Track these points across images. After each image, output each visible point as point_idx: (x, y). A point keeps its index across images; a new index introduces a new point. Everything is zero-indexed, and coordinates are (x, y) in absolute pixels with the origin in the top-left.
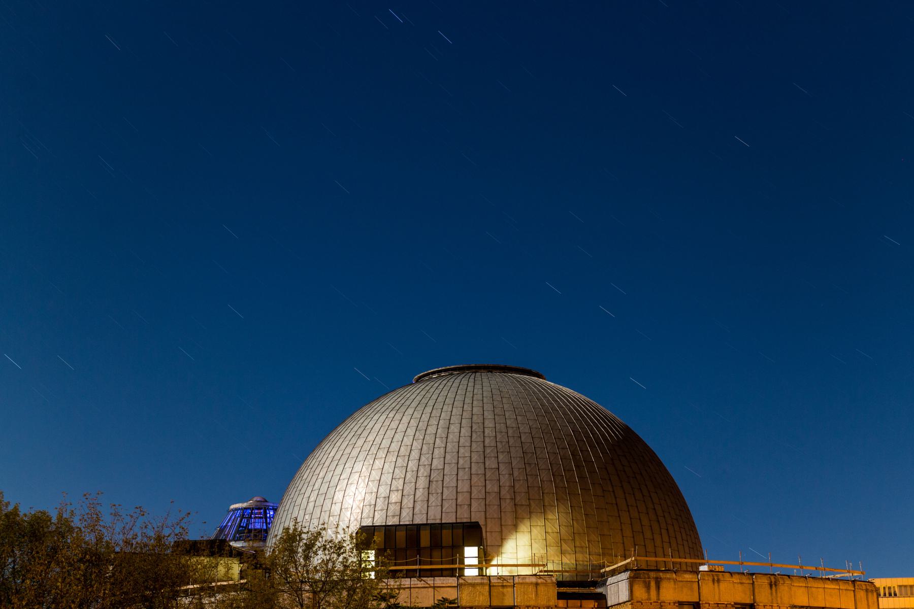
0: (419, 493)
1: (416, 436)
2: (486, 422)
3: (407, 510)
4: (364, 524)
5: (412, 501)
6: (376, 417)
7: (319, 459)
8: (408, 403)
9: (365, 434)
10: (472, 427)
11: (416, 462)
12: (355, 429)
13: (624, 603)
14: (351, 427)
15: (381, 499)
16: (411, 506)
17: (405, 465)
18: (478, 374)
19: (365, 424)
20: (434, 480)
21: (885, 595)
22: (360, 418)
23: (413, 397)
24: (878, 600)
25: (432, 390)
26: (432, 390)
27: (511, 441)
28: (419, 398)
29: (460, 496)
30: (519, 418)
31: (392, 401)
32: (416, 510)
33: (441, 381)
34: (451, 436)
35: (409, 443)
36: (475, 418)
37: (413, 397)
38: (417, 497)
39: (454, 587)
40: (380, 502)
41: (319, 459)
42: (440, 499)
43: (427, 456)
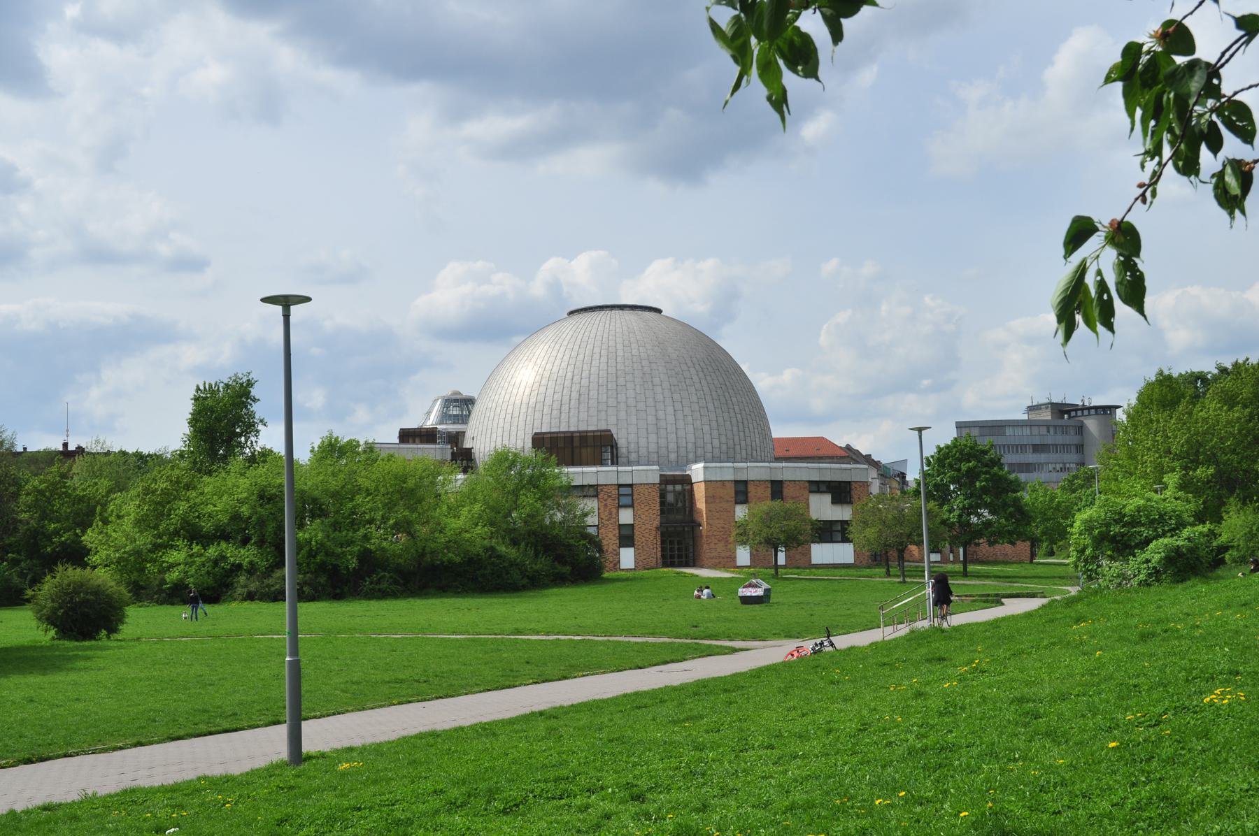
0: (573, 402)
2: (618, 352)
8: (564, 336)
9: (534, 359)
11: (570, 381)
12: (528, 354)
18: (613, 312)
21: (1004, 447)
23: (567, 331)
24: (623, 570)
25: (581, 326)
26: (581, 326)
27: (635, 365)
28: (571, 333)
29: (574, 385)
30: (641, 348)
32: (571, 414)
34: (594, 362)
35: (565, 367)
37: (567, 331)
39: (287, 317)
40: (555, 412)
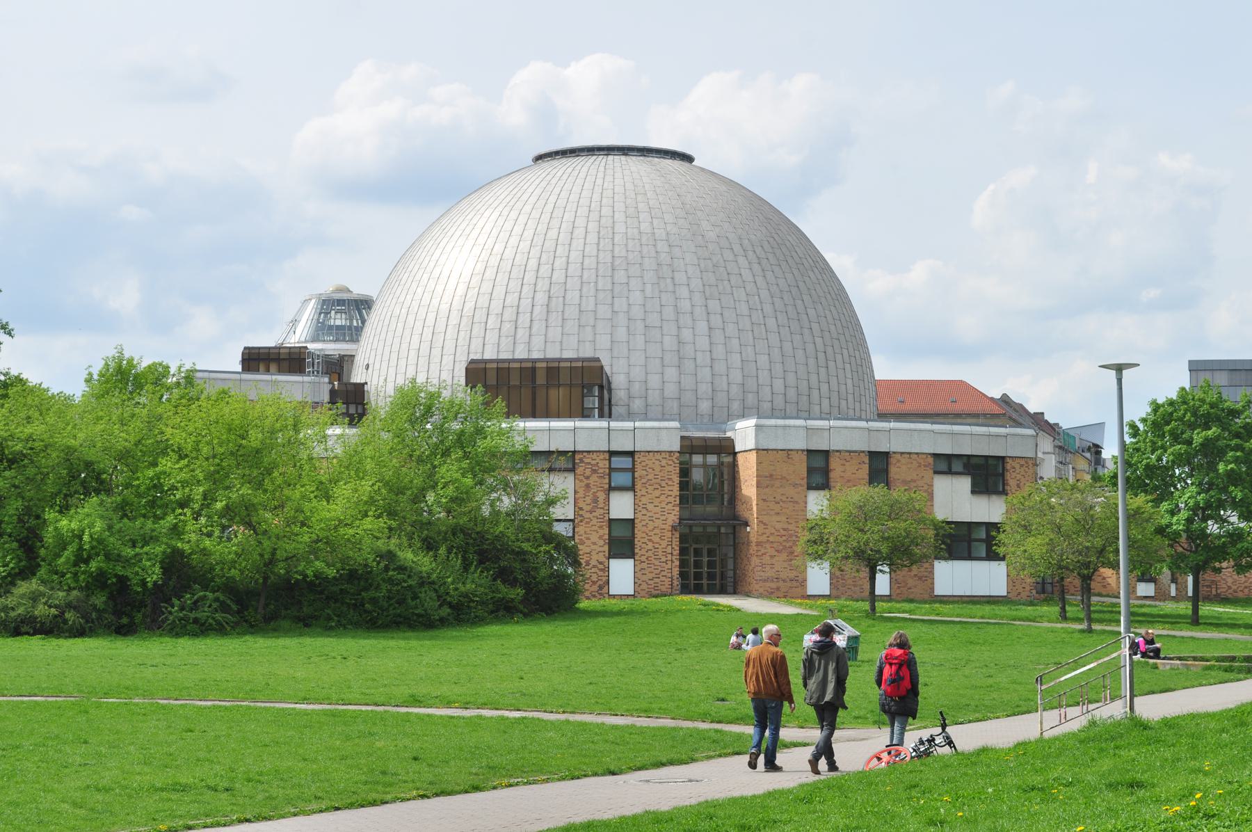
0: (537, 310)
1: (534, 241)
3: (523, 346)
4: (473, 356)
5: (529, 320)
6: (487, 214)
7: (420, 261)
10: (599, 232)
13: (750, 450)
14: (458, 223)
15: (493, 316)
16: (528, 325)
17: (522, 277)
18: (610, 158)
19: (474, 221)
20: (555, 295)
22: (469, 211)
23: (530, 190)
29: (585, 273)
30: (655, 222)
31: (506, 193)
32: (534, 330)
33: (565, 168)
35: (526, 250)
36: (603, 220)
37: (530, 190)
38: (534, 315)
41: (420, 261)
42: (560, 318)
43: (547, 266)
